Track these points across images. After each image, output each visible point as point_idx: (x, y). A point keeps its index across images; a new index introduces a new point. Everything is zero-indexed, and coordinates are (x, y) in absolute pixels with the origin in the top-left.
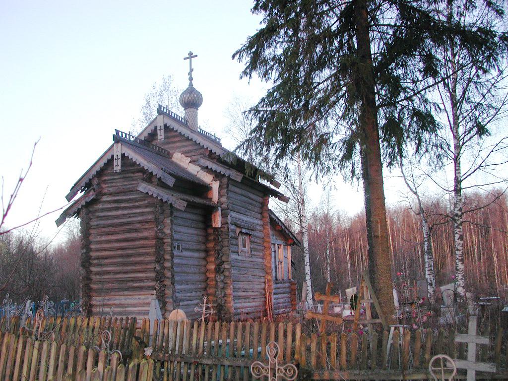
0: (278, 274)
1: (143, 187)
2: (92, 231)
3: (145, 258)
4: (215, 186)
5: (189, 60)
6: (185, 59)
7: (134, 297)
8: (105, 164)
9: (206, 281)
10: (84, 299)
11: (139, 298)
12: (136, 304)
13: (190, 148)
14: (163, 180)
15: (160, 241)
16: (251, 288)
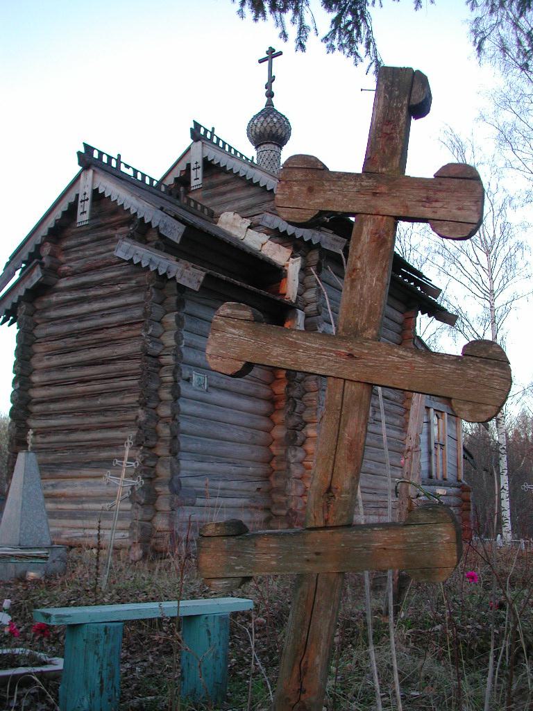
0: (434, 467)
1: (126, 249)
2: (39, 349)
3: (123, 398)
4: (293, 268)
5: (267, 62)
6: (261, 61)
8: (64, 213)
9: (269, 463)
12: (102, 496)
13: (251, 201)
14: (162, 232)
15: (152, 361)
16: (371, 485)
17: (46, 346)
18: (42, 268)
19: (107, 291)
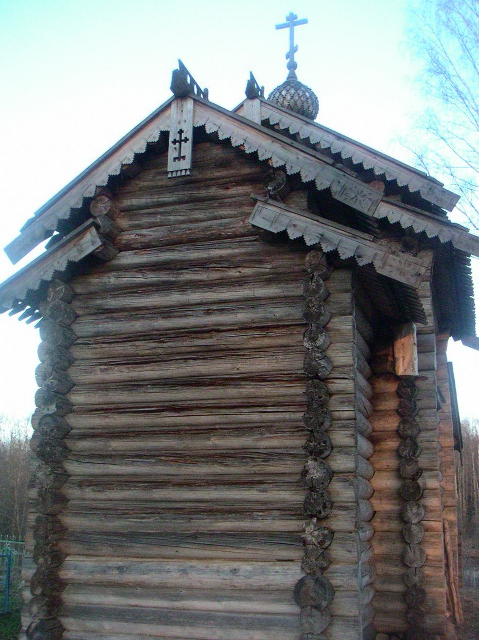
5: (287, 30)
6: (279, 27)
7: (215, 565)
8: (138, 156)
10: (41, 560)
11: (234, 571)
12: (219, 589)
17: (97, 350)
18: (99, 233)
19: (214, 275)
